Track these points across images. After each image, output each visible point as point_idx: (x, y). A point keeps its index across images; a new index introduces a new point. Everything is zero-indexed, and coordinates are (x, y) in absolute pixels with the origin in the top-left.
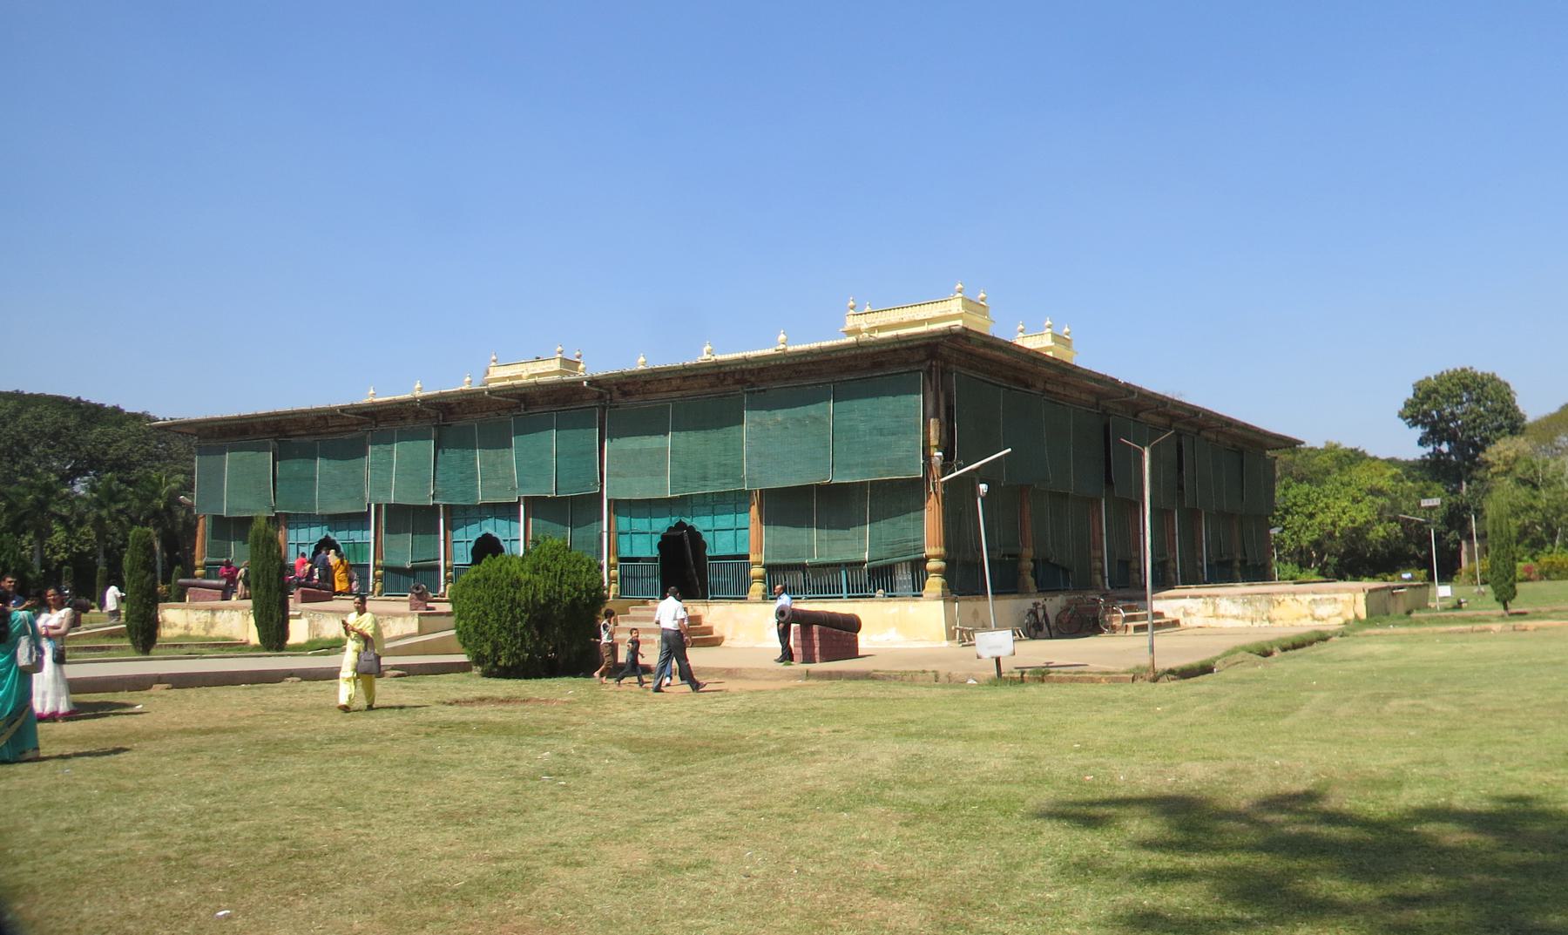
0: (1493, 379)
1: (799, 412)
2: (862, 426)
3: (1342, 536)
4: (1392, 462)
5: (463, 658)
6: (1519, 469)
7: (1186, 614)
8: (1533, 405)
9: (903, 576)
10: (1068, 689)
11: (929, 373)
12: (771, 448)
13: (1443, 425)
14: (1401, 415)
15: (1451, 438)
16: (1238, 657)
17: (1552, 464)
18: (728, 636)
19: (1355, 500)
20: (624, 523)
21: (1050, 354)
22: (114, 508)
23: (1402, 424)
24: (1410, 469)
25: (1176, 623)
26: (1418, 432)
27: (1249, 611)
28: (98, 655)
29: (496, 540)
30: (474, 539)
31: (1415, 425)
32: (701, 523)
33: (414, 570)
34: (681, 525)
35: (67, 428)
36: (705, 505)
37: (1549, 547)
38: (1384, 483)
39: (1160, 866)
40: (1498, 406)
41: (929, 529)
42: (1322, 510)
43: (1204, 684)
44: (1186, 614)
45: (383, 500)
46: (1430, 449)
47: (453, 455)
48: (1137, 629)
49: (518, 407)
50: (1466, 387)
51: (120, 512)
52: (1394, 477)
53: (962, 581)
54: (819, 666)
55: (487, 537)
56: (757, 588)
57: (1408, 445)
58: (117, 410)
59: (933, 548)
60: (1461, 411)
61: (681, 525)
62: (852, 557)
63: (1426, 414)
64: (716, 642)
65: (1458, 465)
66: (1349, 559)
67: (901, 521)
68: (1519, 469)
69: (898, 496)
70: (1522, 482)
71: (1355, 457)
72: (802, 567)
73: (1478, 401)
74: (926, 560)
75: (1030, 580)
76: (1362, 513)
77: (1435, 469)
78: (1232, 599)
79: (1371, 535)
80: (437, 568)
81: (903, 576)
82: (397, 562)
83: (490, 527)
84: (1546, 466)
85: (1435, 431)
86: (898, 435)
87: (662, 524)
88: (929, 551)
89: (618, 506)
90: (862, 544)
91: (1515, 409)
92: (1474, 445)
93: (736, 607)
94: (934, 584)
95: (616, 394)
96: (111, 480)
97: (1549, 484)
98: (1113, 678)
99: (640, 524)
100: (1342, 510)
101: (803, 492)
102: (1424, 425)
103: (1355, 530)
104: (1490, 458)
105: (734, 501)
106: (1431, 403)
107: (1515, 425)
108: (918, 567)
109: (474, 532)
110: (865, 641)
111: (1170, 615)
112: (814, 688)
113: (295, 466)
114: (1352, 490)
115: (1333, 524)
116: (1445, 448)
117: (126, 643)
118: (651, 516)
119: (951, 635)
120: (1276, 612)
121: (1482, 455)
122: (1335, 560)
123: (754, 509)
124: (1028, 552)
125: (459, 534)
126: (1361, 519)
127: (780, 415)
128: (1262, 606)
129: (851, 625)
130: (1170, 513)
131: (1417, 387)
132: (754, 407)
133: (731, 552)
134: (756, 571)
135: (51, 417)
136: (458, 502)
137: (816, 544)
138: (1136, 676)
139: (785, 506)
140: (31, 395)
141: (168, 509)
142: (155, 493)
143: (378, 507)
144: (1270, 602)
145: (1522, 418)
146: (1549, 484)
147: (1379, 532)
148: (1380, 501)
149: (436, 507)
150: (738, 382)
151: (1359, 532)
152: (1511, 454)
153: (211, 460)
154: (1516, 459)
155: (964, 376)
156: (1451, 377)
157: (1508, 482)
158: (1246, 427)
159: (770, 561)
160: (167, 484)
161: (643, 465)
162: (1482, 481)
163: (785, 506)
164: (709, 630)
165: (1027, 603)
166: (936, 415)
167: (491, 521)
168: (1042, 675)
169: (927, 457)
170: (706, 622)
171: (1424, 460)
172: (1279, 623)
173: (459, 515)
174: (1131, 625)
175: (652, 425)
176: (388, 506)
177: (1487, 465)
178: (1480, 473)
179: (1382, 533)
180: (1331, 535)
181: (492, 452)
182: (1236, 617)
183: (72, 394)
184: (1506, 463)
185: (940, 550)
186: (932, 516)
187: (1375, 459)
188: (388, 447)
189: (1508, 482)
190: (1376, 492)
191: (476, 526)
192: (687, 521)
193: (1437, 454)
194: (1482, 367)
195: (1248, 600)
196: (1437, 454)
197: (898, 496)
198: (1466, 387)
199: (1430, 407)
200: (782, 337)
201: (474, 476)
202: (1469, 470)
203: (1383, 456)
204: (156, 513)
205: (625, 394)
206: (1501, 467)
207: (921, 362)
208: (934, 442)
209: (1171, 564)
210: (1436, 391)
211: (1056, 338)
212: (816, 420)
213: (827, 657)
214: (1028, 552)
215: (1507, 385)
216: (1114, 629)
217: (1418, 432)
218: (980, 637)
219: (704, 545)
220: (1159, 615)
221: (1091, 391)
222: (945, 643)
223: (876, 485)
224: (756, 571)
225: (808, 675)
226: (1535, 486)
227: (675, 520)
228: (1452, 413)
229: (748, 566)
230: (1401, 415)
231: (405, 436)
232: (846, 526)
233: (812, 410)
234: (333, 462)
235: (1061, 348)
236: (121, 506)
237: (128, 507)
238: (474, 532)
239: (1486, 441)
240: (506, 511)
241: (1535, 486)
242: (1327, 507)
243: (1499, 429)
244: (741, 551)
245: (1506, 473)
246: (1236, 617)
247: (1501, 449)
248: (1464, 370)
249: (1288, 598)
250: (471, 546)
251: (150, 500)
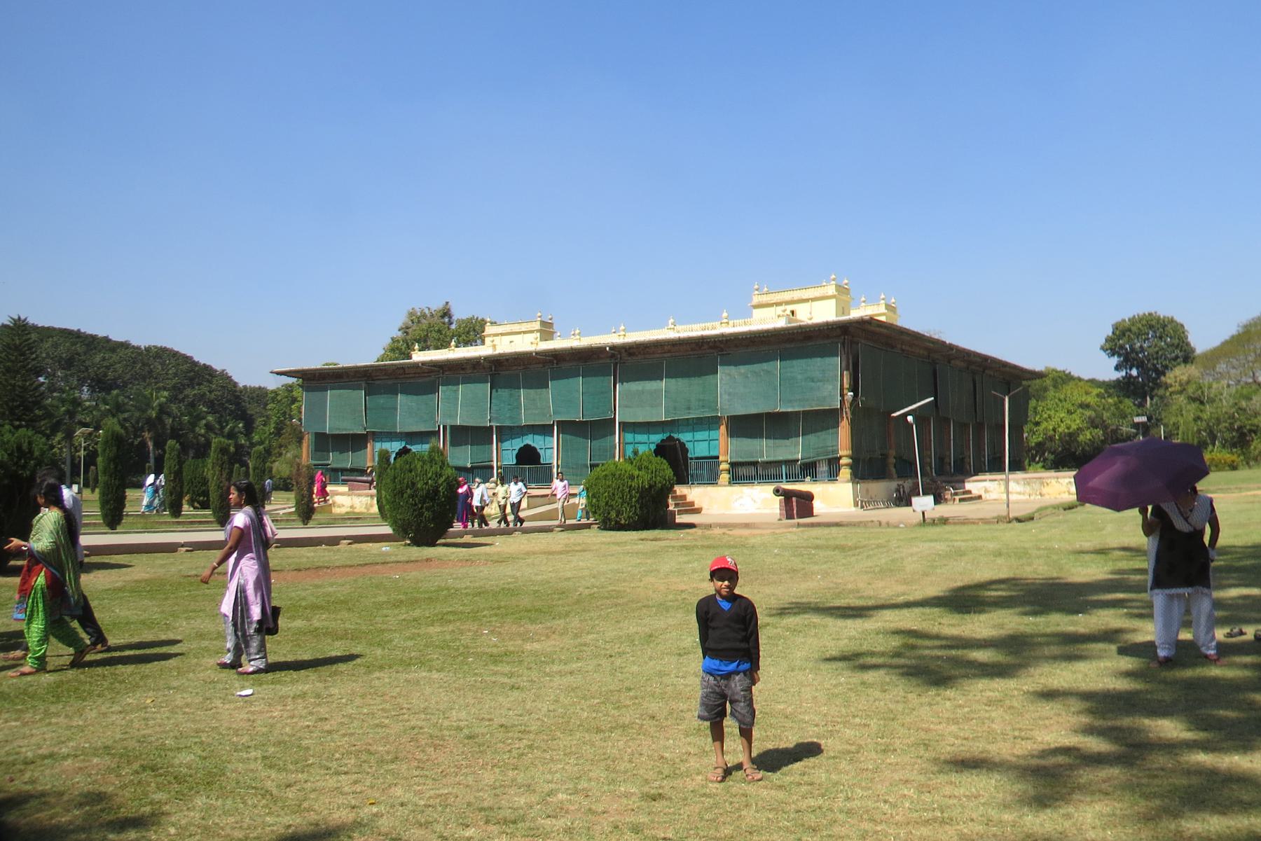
0: (1172, 321)
1: (757, 367)
2: (799, 377)
3: (1060, 439)
4: (1093, 382)
5: (387, 530)
6: (1191, 390)
7: (986, 491)
8: (1202, 339)
9: (823, 468)
10: (958, 528)
11: (843, 344)
12: (735, 390)
13: (1133, 355)
14: (1102, 348)
15: (1141, 365)
16: (1048, 511)
17: (1215, 386)
18: (705, 506)
19: (1070, 412)
20: (629, 437)
21: (883, 319)
22: (122, 416)
23: (1103, 354)
24: (1107, 386)
25: (980, 497)
26: (1115, 360)
27: (1028, 489)
28: (196, 527)
29: (534, 449)
30: (517, 448)
31: (1113, 355)
32: (685, 437)
33: (473, 468)
34: (670, 438)
35: (78, 354)
36: (688, 425)
37: (1210, 447)
38: (1091, 400)
39: (812, 759)
40: (1176, 341)
41: (842, 440)
42: (1046, 420)
43: (1029, 525)
44: (986, 491)
45: (449, 422)
46: (1123, 373)
47: (504, 393)
48: (961, 500)
49: (551, 362)
50: (1151, 327)
51: (125, 420)
52: (1098, 395)
53: (866, 469)
54: (796, 521)
55: (527, 447)
56: (725, 477)
57: (1107, 369)
58: (107, 340)
59: (844, 451)
60: (1146, 345)
61: (670, 438)
62: (790, 457)
63: (1122, 347)
64: (698, 511)
65: (1144, 385)
66: (1064, 455)
67: (822, 435)
68: (1191, 390)
69: (823, 419)
70: (1193, 399)
71: (1064, 379)
72: (755, 464)
73: (1161, 338)
74: (840, 458)
75: (894, 470)
76: (1075, 422)
77: (1125, 388)
78: (1017, 482)
79: (1081, 438)
80: (492, 467)
81: (823, 468)
82: (460, 463)
83: (529, 440)
84: (1210, 387)
85: (1128, 359)
86: (828, 383)
87: (657, 438)
88: (841, 453)
89: (625, 426)
90: (796, 449)
91: (1188, 344)
92: (1156, 370)
93: (710, 489)
94: (845, 473)
95: (624, 354)
96: (118, 395)
97: (1211, 401)
98: (985, 521)
99: (641, 438)
100: (1055, 419)
101: (758, 417)
102: (1119, 356)
103: (1070, 435)
104: (1169, 381)
105: (710, 423)
106: (1126, 339)
107: (1187, 356)
108: (834, 464)
109: (518, 444)
110: (818, 506)
111: (975, 492)
112: (794, 532)
113: (382, 400)
114: (1068, 406)
115: (1054, 430)
116: (1134, 372)
117: (294, 517)
118: (693, 430)
119: (856, 504)
120: (1045, 490)
121: (1163, 378)
122: (1052, 457)
123: (723, 428)
124: (893, 452)
125: (507, 445)
126: (1074, 427)
127: (743, 369)
128: (1036, 486)
129: (808, 498)
130: (966, 426)
131: (1116, 327)
132: (724, 364)
133: (706, 454)
134: (724, 466)
135: (63, 351)
136: (507, 423)
137: (765, 449)
138: (999, 520)
139: (743, 426)
140: (43, 327)
141: (159, 418)
142: (149, 405)
143: (445, 427)
144: (1042, 484)
145: (1193, 351)
146: (1211, 401)
147: (1086, 436)
148: (1088, 413)
149: (491, 427)
150: (711, 348)
151: (1072, 436)
152: (1185, 378)
153: (316, 395)
154: (1188, 382)
155: (868, 348)
156: (1141, 320)
157: (1182, 399)
158: (1015, 367)
159: (734, 460)
160: (157, 398)
161: (652, 400)
162: (1162, 398)
163: (743, 426)
164: (692, 504)
165: (893, 485)
166: (847, 369)
167: (531, 436)
168: (944, 521)
169: (842, 395)
170: (689, 499)
171: (1118, 380)
172: (1047, 497)
173: (506, 433)
174: (957, 498)
175: (655, 375)
176: (452, 427)
177: (1167, 386)
178: (1161, 392)
179: (1089, 436)
180: (1051, 439)
181: (532, 391)
182: (1020, 493)
183: (73, 326)
184: (1181, 385)
185: (849, 452)
186: (844, 432)
187: (1080, 379)
188: (514, 392)
189: (1182, 399)
190: (1085, 406)
191: (518, 440)
192: (676, 436)
193: (1129, 377)
194: (1164, 311)
195: (1027, 482)
196: (1129, 377)
197: (823, 419)
198: (1151, 327)
199: (1123, 342)
200: (725, 314)
201: (519, 407)
202: (1152, 389)
203: (1086, 377)
204: (149, 421)
205: (630, 354)
206: (1178, 388)
207: (838, 336)
208: (846, 385)
209: (967, 460)
210: (1130, 330)
211: (888, 307)
212: (768, 372)
213: (800, 516)
214: (893, 452)
215: (1182, 326)
216: (946, 500)
217: (1115, 360)
218: (915, 500)
219: (687, 451)
220: (970, 492)
221: (927, 349)
222: (854, 509)
223: (806, 414)
224: (724, 466)
225: (799, 525)
226: (1202, 403)
227: (665, 436)
228: (1141, 347)
229: (719, 464)
230: (1102, 348)
231: (466, 381)
232: (787, 437)
233: (765, 366)
234: (410, 397)
235: (891, 314)
236: (126, 415)
237: (131, 417)
238: (518, 444)
239: (1166, 367)
240: (545, 430)
241: (1202, 403)
242: (1050, 417)
243: (1177, 357)
244: (713, 453)
245: (1181, 392)
246: (1020, 493)
247: (1177, 375)
248: (1150, 314)
249: (1054, 481)
250: (515, 453)
251: (144, 411)
